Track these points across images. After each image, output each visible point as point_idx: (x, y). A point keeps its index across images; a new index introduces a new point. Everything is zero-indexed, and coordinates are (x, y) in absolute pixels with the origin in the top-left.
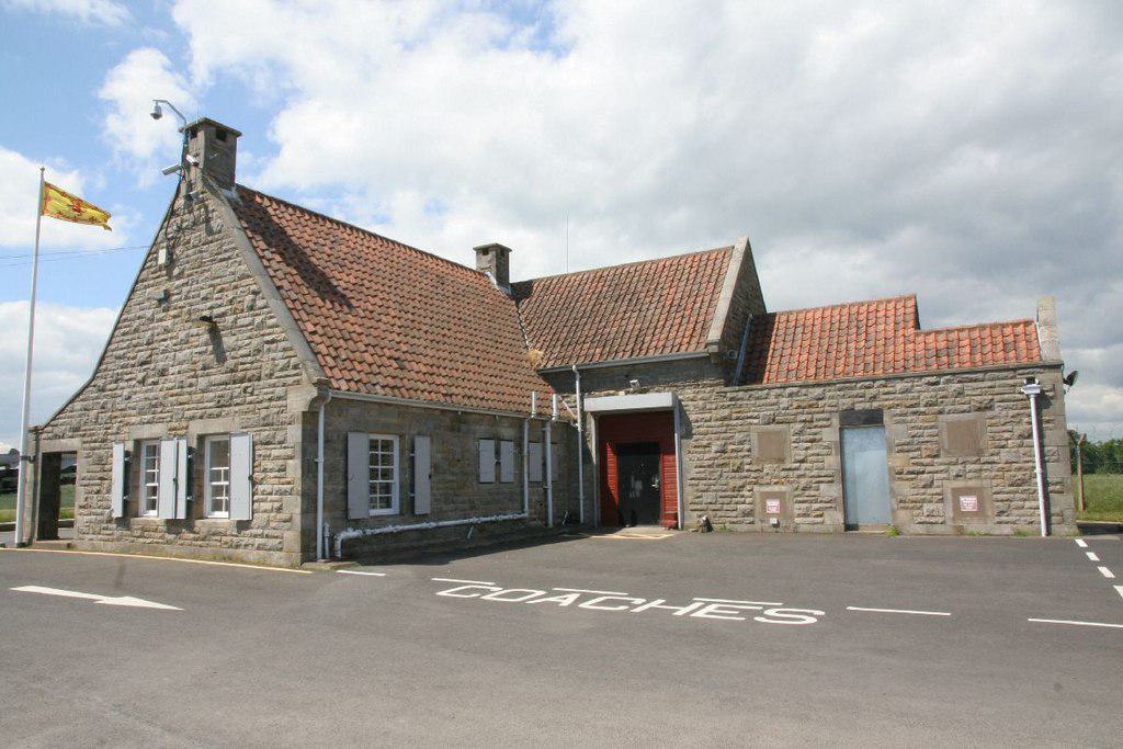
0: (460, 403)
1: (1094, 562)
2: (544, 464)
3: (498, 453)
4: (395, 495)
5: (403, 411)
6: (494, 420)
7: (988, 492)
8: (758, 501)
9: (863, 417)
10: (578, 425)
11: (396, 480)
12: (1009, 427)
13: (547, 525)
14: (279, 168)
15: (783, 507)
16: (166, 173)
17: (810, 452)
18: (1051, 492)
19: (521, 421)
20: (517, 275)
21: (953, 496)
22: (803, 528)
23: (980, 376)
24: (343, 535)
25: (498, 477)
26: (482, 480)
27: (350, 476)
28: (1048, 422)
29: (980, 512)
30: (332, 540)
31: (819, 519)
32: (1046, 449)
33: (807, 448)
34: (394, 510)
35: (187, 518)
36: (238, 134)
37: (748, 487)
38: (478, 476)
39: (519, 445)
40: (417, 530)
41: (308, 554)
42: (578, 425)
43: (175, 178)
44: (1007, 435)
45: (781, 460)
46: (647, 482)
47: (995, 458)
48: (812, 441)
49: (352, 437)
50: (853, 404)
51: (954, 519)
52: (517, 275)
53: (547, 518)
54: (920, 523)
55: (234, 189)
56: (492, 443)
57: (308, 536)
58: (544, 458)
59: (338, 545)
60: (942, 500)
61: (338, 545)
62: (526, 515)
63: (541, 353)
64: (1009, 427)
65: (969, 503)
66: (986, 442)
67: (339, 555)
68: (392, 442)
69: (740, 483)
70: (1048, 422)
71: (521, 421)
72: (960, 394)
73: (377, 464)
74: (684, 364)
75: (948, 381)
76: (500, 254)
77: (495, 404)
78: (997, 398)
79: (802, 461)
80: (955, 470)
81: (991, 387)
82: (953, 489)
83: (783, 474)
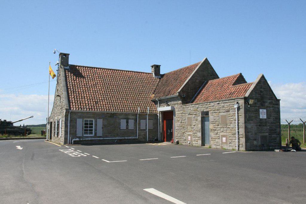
0: (112, 110)
1: (22, 149)
2: (146, 125)
3: (127, 122)
4: (93, 132)
5: (94, 114)
6: (126, 114)
7: (228, 137)
8: (187, 136)
9: (205, 113)
10: (158, 115)
11: (93, 129)
12: (232, 117)
13: (147, 141)
14: (72, 61)
15: (191, 138)
16: (56, 65)
17: (196, 123)
18: (240, 137)
19: (137, 114)
20: (162, 72)
21: (221, 137)
22: (194, 145)
23: (227, 101)
24: (74, 140)
25: (127, 128)
26: (121, 129)
27: (77, 128)
28: (240, 116)
29: (226, 143)
30: (71, 140)
31: (197, 142)
32: (239, 124)
33: (195, 122)
34: (93, 135)
35: (97, 136)
36: (69, 54)
37: (185, 133)
38: (120, 128)
39: (136, 120)
40: (97, 139)
41: (65, 143)
42: (158, 115)
43: (57, 65)
44: (232, 120)
45: (191, 125)
46: (170, 130)
47: (230, 127)
48: (196, 120)
49: (78, 120)
50: (204, 110)
51: (221, 144)
52: (162, 72)
53: (146, 139)
54: (215, 145)
55: (68, 66)
56: (125, 120)
57: (66, 139)
58: (146, 123)
59: (73, 141)
60: (219, 139)
61: (73, 141)
62: (137, 138)
63: (154, 95)
64: (232, 117)
65: (224, 139)
66: (228, 122)
67: (73, 143)
68: (93, 120)
69: (184, 131)
70: (240, 116)
71: (137, 114)
72: (223, 107)
73: (88, 126)
74: (175, 98)
75: (221, 103)
76: (157, 68)
77: (126, 110)
78: (231, 108)
79: (194, 126)
80: (222, 129)
81: (229, 105)
82: (221, 135)
83: (191, 129)
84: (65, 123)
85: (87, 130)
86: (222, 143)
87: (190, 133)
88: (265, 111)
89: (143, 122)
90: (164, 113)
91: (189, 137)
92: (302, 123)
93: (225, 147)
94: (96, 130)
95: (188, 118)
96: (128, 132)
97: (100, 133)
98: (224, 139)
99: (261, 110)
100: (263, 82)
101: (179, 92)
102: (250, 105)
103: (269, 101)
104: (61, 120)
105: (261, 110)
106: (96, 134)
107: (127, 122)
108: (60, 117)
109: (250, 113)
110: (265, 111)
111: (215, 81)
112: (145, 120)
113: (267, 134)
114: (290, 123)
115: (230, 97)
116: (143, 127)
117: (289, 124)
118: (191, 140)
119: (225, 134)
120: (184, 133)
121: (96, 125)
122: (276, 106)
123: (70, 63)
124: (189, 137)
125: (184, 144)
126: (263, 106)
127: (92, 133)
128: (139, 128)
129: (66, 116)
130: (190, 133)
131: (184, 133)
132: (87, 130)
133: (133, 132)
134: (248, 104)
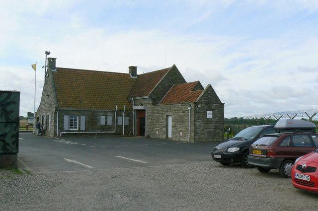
3: (106, 119)
29: (182, 136)
34: (77, 129)
43: (44, 68)
65: (181, 133)
72: (181, 108)
84: (55, 119)
85: (72, 125)
86: (180, 136)
87: (157, 129)
88: (211, 112)
89: (120, 118)
90: (138, 111)
91: (157, 132)
92: (309, 118)
93: (182, 140)
94: (80, 125)
95: (157, 116)
96: (106, 127)
97: (83, 128)
98: (181, 133)
99: (208, 112)
100: (210, 87)
101: (150, 95)
102: (199, 108)
103: (215, 105)
104: (50, 116)
105: (208, 112)
106: (79, 128)
107: (106, 119)
108: (48, 114)
109: (199, 114)
110: (211, 112)
111: (182, 85)
112: (121, 117)
113: (212, 130)
114: (312, 117)
115: (188, 100)
116: (120, 123)
117: (310, 118)
118: (159, 135)
119: (182, 129)
120: (153, 128)
121: (80, 121)
122: (221, 109)
123: (57, 66)
124: (157, 132)
125: (153, 137)
126: (209, 109)
127: (76, 128)
128: (116, 124)
129: (56, 113)
130: (157, 129)
131: (153, 128)
132: (72, 125)
133: (110, 128)
134: (198, 107)
